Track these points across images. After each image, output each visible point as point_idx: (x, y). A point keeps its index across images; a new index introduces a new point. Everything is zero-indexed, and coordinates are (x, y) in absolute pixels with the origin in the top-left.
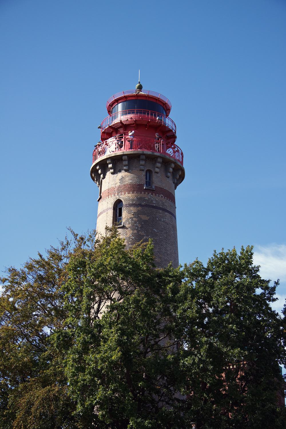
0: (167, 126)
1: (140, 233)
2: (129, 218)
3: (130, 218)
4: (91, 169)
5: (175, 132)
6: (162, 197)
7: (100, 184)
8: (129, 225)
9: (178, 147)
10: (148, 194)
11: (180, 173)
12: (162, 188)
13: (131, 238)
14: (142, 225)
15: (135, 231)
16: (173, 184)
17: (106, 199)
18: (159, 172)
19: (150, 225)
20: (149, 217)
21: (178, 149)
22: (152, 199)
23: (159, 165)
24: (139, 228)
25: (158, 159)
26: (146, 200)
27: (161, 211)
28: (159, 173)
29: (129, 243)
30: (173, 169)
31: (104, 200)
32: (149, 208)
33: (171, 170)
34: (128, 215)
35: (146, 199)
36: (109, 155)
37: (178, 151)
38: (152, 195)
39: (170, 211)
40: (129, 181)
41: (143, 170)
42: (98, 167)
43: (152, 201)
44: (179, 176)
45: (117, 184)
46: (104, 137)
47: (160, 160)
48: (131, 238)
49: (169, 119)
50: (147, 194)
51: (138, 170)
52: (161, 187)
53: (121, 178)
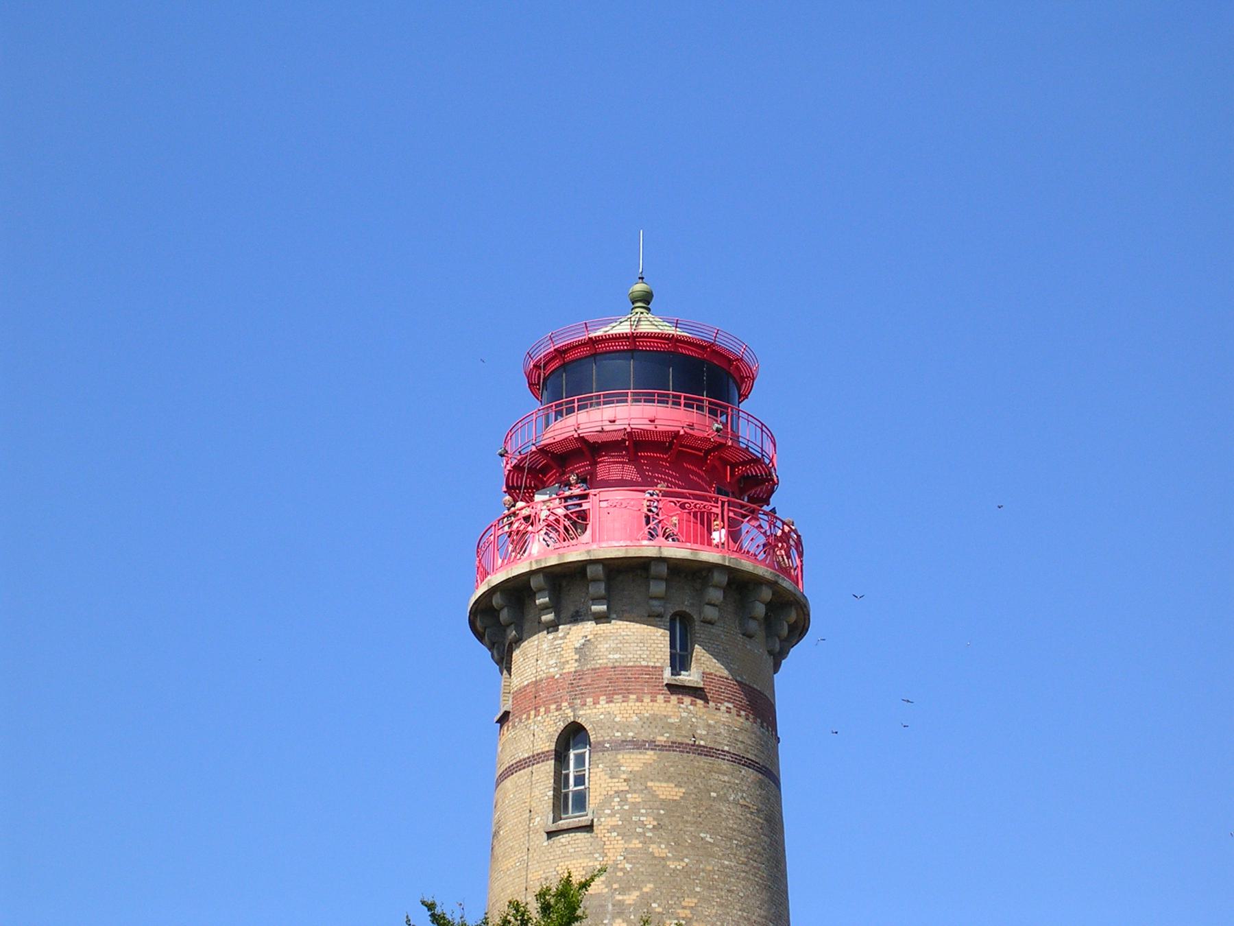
0: (745, 446)
1: (653, 848)
2: (613, 793)
3: (616, 792)
4: (471, 605)
7: (504, 661)
8: (614, 819)
11: (793, 616)
13: (620, 866)
14: (657, 818)
15: (543, 551)
16: (765, 655)
18: (715, 622)
23: (715, 595)
25: (713, 573)
28: (716, 624)
29: (615, 886)
32: (685, 755)
38: (691, 707)
40: (611, 656)
44: (789, 625)
45: (568, 666)
48: (621, 870)
49: (750, 418)
50: (676, 702)
51: (644, 616)
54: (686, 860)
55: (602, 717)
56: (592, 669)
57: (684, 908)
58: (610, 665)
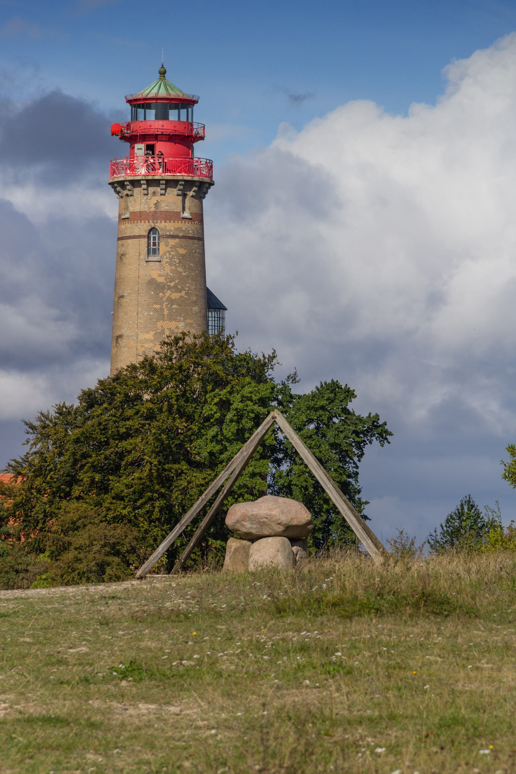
1: (178, 269)
10: (185, 223)
17: (137, 223)
31: (134, 223)
43: (189, 231)
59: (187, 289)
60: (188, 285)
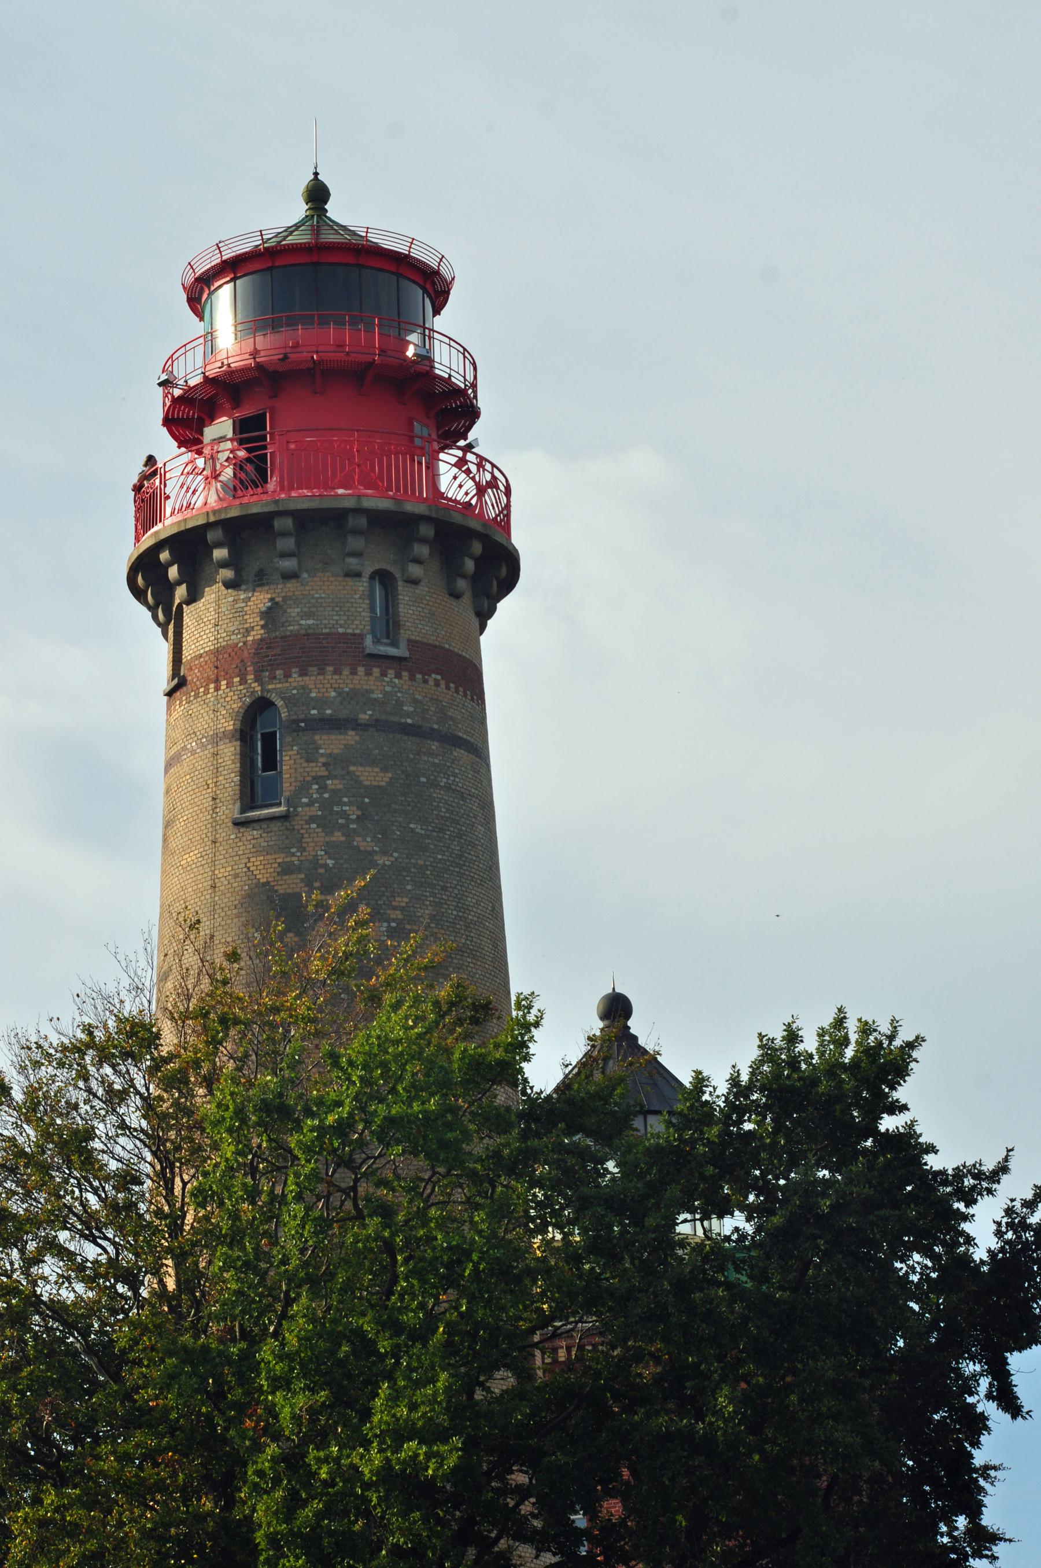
0: (446, 376)
5: (475, 397)
6: (437, 684)
9: (493, 466)
10: (384, 674)
12: (435, 647)
14: (361, 807)
19: (397, 807)
20: (390, 775)
21: (492, 473)
22: (399, 695)
23: (423, 550)
24: (353, 821)
26: (375, 699)
27: (435, 746)
28: (421, 583)
30: (477, 561)
31: (196, 696)
32: (391, 736)
33: (470, 565)
34: (306, 765)
35: (375, 696)
36: (215, 512)
37: (493, 484)
38: (396, 681)
39: (469, 738)
40: (303, 622)
41: (358, 575)
42: (164, 556)
45: (253, 633)
46: (178, 414)
47: (427, 530)
49: (452, 343)
52: (432, 640)
53: (269, 608)
54: (395, 855)
55: (295, 692)
56: (282, 637)
57: (395, 908)
58: (302, 632)
59: (398, 914)
60: (402, 901)
